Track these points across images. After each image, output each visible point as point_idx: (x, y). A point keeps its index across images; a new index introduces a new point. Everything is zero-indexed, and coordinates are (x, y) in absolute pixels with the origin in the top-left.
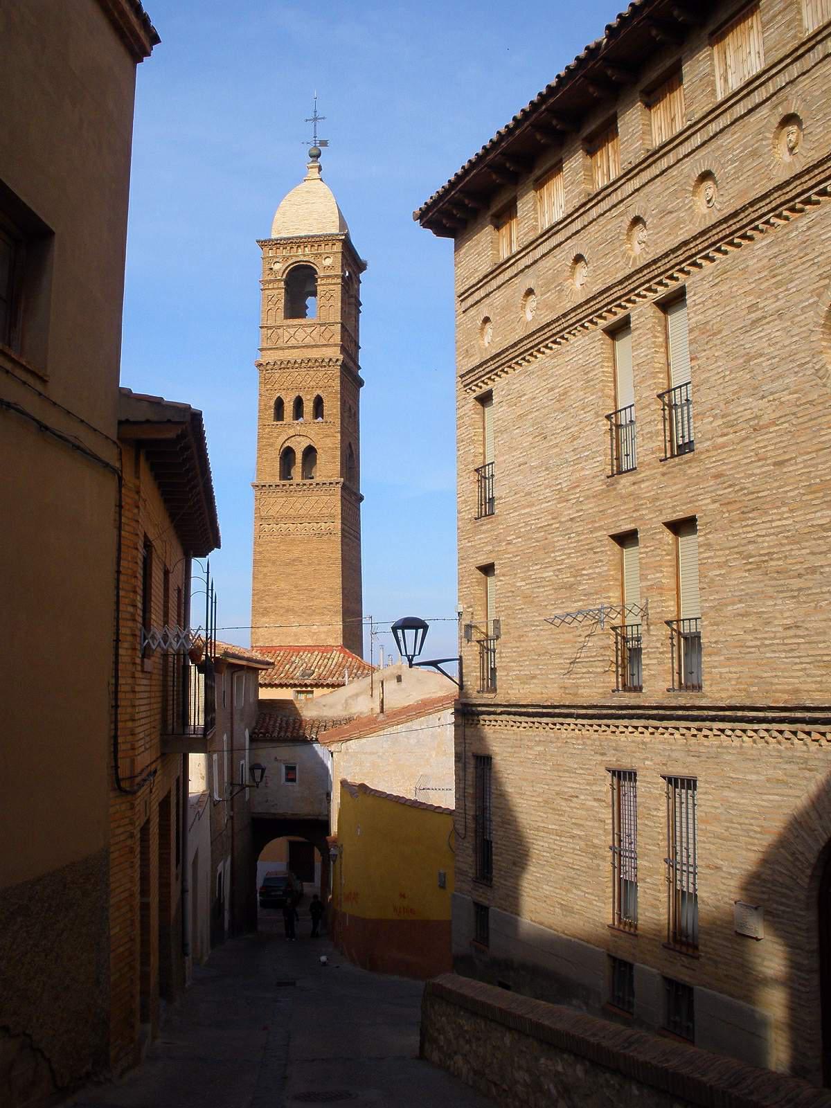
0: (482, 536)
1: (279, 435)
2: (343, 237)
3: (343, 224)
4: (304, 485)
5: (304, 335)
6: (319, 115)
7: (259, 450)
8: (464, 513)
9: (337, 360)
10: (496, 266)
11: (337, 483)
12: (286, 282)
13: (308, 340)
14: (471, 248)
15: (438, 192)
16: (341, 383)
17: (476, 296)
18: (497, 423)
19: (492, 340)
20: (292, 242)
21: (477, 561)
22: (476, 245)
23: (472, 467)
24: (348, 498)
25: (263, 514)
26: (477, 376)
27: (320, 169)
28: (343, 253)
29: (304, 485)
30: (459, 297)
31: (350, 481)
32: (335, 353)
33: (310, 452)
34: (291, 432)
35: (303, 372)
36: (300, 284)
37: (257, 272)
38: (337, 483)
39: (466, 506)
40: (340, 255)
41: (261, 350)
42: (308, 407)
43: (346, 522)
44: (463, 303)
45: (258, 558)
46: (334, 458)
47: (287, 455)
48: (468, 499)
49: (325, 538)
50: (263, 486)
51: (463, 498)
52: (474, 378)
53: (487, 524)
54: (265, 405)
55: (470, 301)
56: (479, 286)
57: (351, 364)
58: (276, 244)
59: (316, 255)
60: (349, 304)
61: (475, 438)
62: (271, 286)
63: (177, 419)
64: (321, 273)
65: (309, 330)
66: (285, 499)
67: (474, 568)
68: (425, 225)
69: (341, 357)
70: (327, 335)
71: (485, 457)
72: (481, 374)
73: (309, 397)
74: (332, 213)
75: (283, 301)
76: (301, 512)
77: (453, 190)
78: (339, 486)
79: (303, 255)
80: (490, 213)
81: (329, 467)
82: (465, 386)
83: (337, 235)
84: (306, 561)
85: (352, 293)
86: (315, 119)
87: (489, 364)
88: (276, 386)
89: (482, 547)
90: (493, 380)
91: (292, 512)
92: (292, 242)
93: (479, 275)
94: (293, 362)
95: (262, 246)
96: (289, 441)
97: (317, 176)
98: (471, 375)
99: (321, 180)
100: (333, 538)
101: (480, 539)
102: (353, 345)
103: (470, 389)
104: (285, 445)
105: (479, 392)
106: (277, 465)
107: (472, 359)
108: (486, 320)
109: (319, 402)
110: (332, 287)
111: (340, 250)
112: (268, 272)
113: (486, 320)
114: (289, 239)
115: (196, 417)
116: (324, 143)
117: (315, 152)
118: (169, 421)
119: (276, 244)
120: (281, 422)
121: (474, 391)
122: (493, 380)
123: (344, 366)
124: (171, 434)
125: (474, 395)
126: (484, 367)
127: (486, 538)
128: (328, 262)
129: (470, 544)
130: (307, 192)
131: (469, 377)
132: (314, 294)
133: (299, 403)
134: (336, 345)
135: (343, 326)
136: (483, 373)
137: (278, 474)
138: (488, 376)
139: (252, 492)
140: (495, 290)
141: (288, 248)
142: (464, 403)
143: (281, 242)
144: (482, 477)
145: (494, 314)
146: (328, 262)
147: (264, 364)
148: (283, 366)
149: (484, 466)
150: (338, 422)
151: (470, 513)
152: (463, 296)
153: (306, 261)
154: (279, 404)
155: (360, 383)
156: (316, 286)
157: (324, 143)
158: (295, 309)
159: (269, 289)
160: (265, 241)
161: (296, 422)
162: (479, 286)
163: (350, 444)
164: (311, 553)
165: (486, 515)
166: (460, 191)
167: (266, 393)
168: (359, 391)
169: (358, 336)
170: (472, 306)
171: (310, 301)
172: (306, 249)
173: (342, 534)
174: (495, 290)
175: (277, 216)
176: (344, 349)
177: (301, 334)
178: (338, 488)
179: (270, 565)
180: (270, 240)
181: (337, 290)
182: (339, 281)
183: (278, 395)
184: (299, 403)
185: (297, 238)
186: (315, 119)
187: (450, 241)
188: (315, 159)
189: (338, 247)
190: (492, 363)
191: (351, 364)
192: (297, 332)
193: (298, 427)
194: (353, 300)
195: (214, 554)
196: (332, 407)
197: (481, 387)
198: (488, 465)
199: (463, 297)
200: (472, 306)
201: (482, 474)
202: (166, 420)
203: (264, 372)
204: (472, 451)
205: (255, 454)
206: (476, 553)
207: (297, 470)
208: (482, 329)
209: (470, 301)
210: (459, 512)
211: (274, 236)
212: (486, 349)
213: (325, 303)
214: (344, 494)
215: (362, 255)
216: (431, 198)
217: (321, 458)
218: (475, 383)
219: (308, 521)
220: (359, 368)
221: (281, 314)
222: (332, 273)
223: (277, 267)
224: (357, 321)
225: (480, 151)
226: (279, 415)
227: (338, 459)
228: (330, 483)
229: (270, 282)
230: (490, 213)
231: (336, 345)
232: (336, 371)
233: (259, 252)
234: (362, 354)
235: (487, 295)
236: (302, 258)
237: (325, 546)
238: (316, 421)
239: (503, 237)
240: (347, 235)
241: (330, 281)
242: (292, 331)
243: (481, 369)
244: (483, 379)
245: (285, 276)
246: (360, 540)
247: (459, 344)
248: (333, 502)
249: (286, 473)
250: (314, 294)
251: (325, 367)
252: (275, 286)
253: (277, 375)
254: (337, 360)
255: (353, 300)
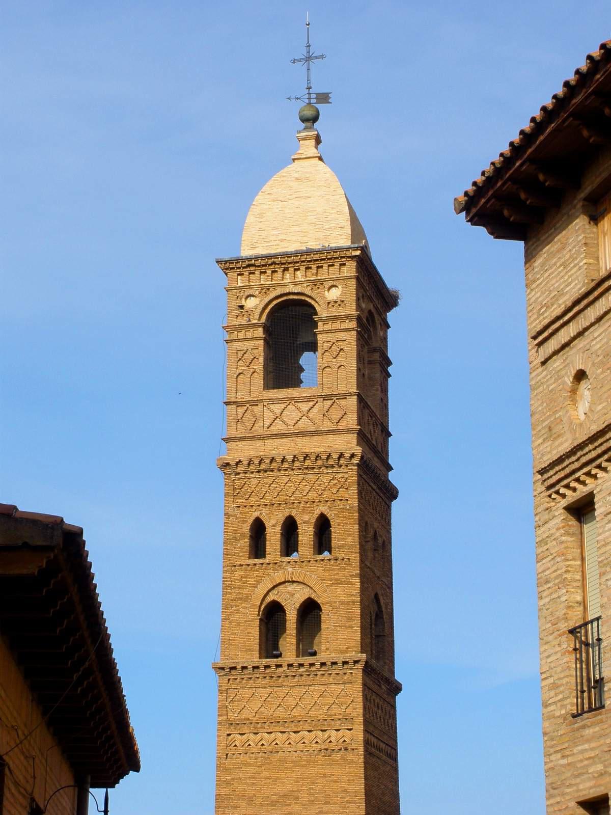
0: (586, 746)
1: (258, 582)
2: (358, 253)
3: (357, 231)
4: (301, 665)
5: (296, 415)
6: (315, 51)
7: (226, 607)
8: (552, 708)
9: (353, 456)
10: (593, 284)
11: (356, 662)
12: (267, 329)
13: (305, 424)
14: (552, 255)
15: (493, 164)
16: (360, 493)
17: (563, 336)
18: (603, 550)
19: (591, 410)
20: (274, 263)
21: (578, 791)
22: (559, 251)
23: (564, 626)
24: (375, 687)
25: (232, 716)
26: (567, 471)
27: (318, 140)
28: (358, 278)
29: (301, 665)
30: (535, 338)
31: (377, 658)
32: (349, 444)
33: (310, 611)
34: (279, 577)
35: (297, 476)
36: (288, 332)
37: (220, 313)
38: (356, 662)
39: (556, 695)
40: (353, 283)
41: (227, 440)
42: (306, 534)
43: (371, 729)
44: (541, 350)
45: (223, 792)
46: (350, 619)
47: (272, 615)
48: (559, 682)
49: (337, 756)
50: (232, 668)
51: (551, 680)
52: (562, 474)
53: (593, 725)
54: (235, 532)
55: (553, 345)
56: (566, 318)
57: (376, 462)
58: (249, 266)
59: (314, 283)
60: (370, 363)
61: (568, 576)
62: (241, 335)
63: (40, 542)
64: (322, 312)
65: (305, 407)
66: (268, 690)
67: (573, 804)
68: (475, 220)
69: (358, 451)
70: (335, 414)
71: (585, 608)
72: (573, 467)
73: (306, 517)
74: (339, 213)
75: (261, 360)
76: (296, 713)
77: (517, 160)
78: (360, 666)
79: (293, 283)
80: (582, 195)
81: (341, 635)
82: (548, 488)
83: (348, 249)
84: (304, 797)
85: (375, 344)
86: (309, 58)
87: (587, 449)
88: (253, 500)
89: (587, 766)
90: (595, 477)
91: (281, 713)
92: (274, 263)
93: (567, 300)
94: (279, 459)
95: (226, 270)
96: (275, 592)
97: (313, 151)
98: (557, 468)
99: (320, 159)
100: (350, 756)
101: (582, 752)
102: (378, 431)
103: (557, 492)
104: (269, 599)
105: (572, 497)
106: (255, 632)
107: (557, 443)
108: (581, 376)
109: (323, 526)
110: (342, 335)
111: (353, 273)
112: (237, 312)
113: (581, 376)
114: (270, 257)
115: (72, 540)
116: (324, 98)
117: (309, 113)
118: (26, 545)
119: (249, 266)
120: (261, 561)
121: (564, 496)
122: (595, 477)
123: (365, 467)
124: (31, 567)
125: (564, 503)
126: (579, 454)
127: (592, 749)
128: (334, 294)
129: (564, 761)
130: (297, 179)
131: (558, 472)
132: (312, 347)
133: (290, 528)
134: (349, 431)
135: (361, 400)
136: (577, 465)
137: (257, 648)
138: (585, 470)
139: (213, 679)
140: (592, 325)
141: (269, 272)
142: (546, 517)
143: (257, 263)
144: (581, 642)
145: (593, 364)
146: (334, 294)
147: (233, 463)
148: (263, 466)
149: (586, 624)
150: (355, 559)
151: (563, 706)
152: (541, 336)
153: (298, 294)
154: (258, 529)
155: (391, 493)
156: (315, 335)
157: (324, 98)
158: (282, 369)
159: (239, 340)
160: (231, 262)
161: (287, 559)
162: (566, 318)
163: (376, 596)
164: (313, 783)
165: (591, 710)
166: (529, 159)
167: (237, 512)
168: (389, 507)
169: (386, 415)
170: (556, 353)
171: (306, 359)
172: (298, 273)
173: (366, 750)
174: (592, 325)
175: (250, 219)
176: (362, 437)
177: (291, 414)
178: (357, 673)
179: (243, 804)
180: (238, 260)
181: (350, 342)
182: (353, 324)
183: (256, 514)
184: (290, 528)
185: (283, 255)
186: (309, 58)
187: (517, 247)
188: (309, 124)
189: (350, 269)
190: (591, 447)
191: (376, 462)
192: (286, 410)
193: (289, 568)
194: (377, 356)
195: (130, 780)
196: (346, 534)
197: (574, 490)
198: (592, 622)
199: (540, 338)
200: (556, 353)
201: (582, 638)
202: (20, 543)
203: (233, 477)
204: (563, 599)
205: (218, 617)
206: (576, 776)
207: (289, 641)
208: (574, 391)
209: (553, 345)
210: (545, 705)
211: (246, 252)
212: (581, 425)
213: (332, 364)
214: (367, 679)
215: (391, 282)
216: (483, 173)
217: (329, 619)
218: (565, 482)
219: (307, 727)
220: (389, 468)
221: (259, 380)
222: (342, 312)
223: (250, 303)
224: (385, 390)
225: (560, 90)
226: (258, 547)
227: (357, 622)
228: (345, 663)
229: (240, 328)
230: (582, 195)
231: (349, 431)
232: (351, 474)
233: (220, 279)
234: (393, 445)
235: (580, 334)
236: (291, 288)
237: (336, 770)
238: (320, 557)
239: (605, 235)
240: (364, 249)
241: (338, 325)
242: (277, 408)
243: (573, 458)
244: (577, 475)
245: (264, 317)
246: (395, 759)
247: (537, 416)
248: (348, 695)
249: (270, 644)
250: (312, 347)
251: (332, 466)
252: (249, 335)
253: (254, 482)
254: (353, 456)
255: (377, 356)
